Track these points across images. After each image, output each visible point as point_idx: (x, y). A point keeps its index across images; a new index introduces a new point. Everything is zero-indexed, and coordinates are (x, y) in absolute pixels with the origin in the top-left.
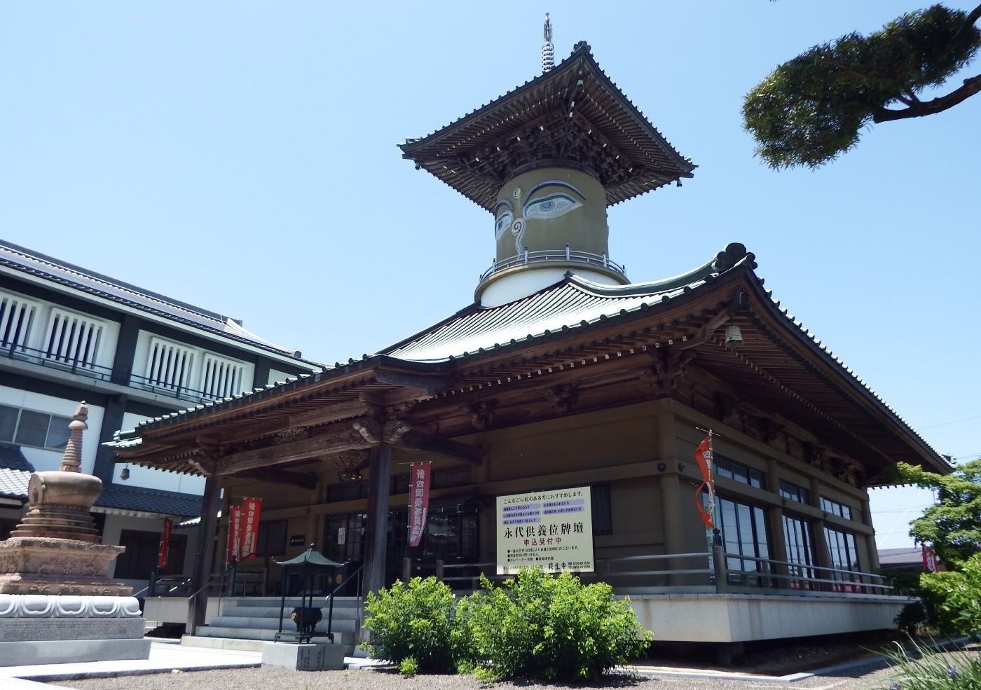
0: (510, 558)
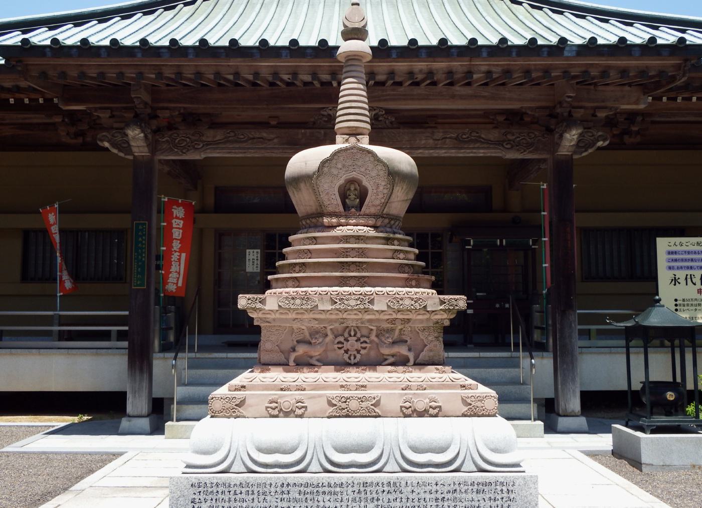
0: (678, 308)
